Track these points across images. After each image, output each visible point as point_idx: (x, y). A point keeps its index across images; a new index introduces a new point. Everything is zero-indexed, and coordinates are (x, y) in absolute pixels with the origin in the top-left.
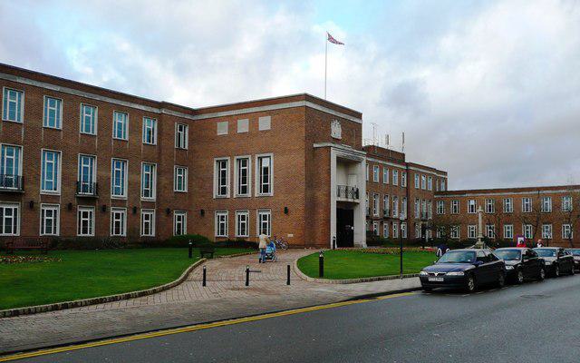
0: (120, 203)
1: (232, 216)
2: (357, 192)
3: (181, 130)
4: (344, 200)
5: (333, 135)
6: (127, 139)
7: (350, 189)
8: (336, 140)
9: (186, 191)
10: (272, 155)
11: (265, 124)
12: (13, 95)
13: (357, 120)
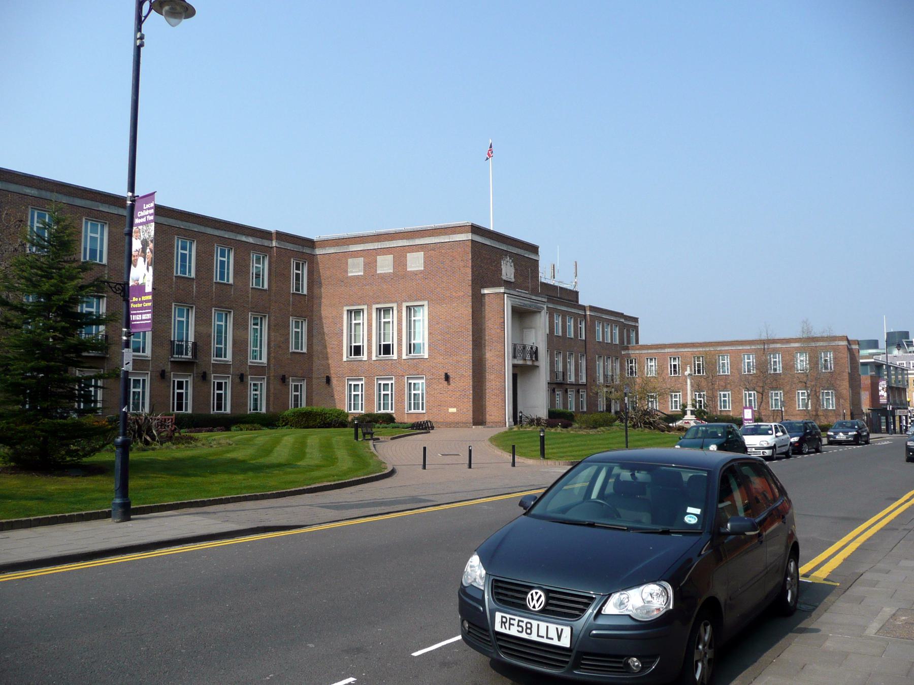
0: (223, 368)
1: (369, 384)
2: (536, 352)
3: (298, 268)
4: (520, 362)
5: (504, 278)
6: (231, 281)
7: (528, 348)
8: (507, 284)
9: (305, 350)
10: (426, 303)
11: (416, 262)
12: (94, 231)
13: (533, 257)
